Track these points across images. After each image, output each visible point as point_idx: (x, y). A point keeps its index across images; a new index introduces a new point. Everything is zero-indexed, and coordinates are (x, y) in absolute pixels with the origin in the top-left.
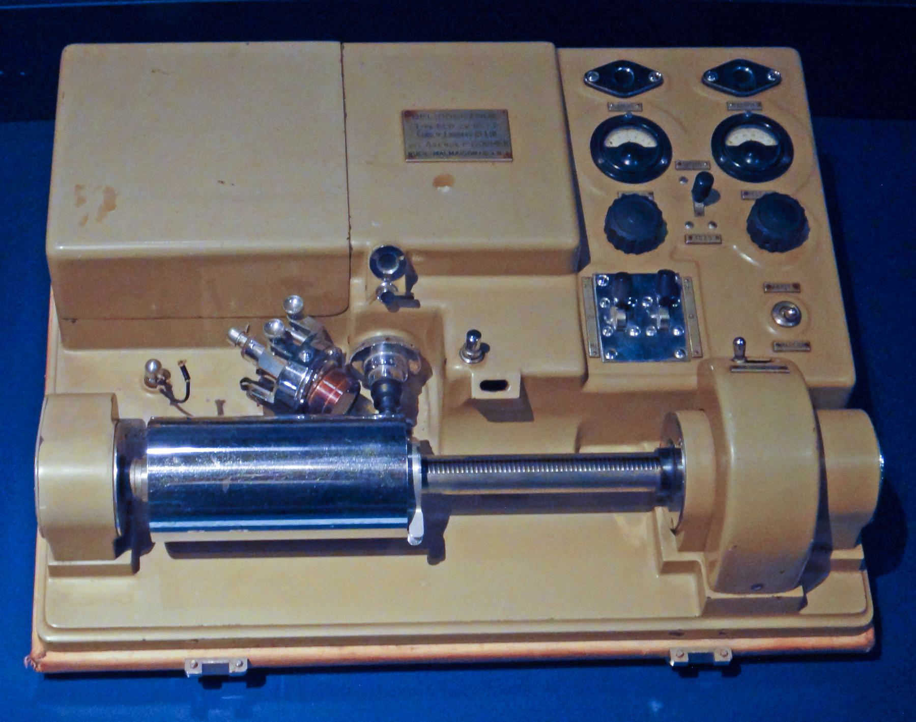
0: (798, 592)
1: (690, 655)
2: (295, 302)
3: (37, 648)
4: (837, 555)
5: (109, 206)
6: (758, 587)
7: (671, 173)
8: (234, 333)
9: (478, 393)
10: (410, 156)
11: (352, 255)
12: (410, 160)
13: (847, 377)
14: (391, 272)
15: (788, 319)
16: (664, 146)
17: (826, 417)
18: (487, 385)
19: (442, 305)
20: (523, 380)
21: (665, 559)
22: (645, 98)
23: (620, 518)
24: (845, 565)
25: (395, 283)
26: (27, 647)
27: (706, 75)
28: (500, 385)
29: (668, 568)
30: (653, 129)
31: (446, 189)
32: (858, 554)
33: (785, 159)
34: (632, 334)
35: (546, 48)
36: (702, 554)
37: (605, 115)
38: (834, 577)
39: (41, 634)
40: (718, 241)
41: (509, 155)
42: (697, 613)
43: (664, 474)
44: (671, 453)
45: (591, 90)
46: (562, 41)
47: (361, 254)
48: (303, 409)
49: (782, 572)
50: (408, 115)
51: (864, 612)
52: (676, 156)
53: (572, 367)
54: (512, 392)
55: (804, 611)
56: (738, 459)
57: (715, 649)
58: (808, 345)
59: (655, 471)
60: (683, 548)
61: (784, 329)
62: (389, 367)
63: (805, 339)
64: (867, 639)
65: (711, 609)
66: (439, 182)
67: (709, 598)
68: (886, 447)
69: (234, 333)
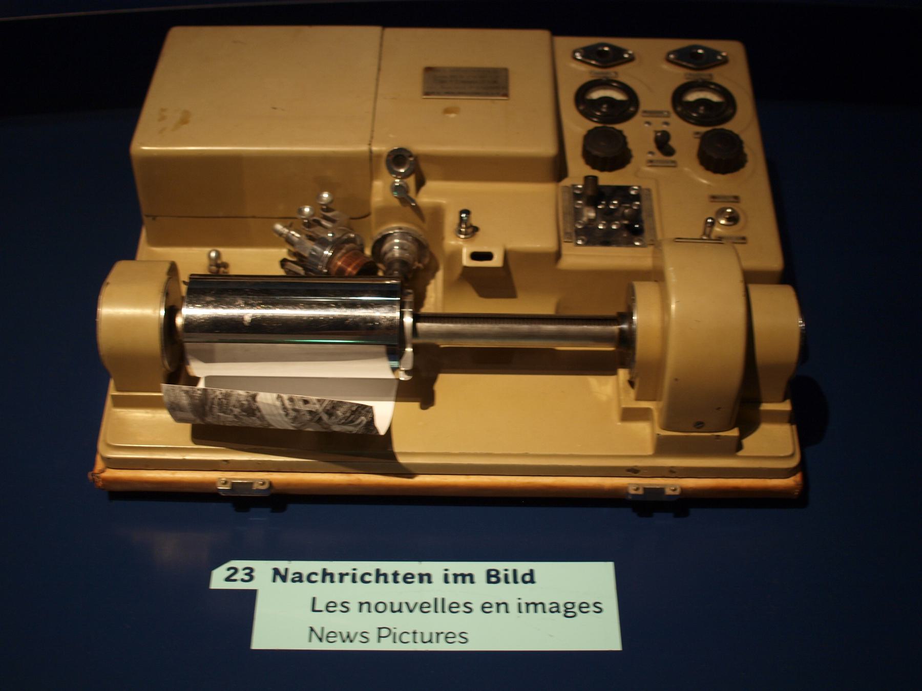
0: (735, 433)
1: (645, 489)
2: (325, 195)
3: (99, 465)
4: (766, 407)
5: (184, 121)
6: (699, 426)
7: (638, 118)
8: (279, 227)
9: (466, 261)
10: (427, 94)
11: (372, 157)
12: (425, 97)
13: (774, 261)
14: (402, 171)
15: (728, 220)
16: (633, 98)
17: (757, 292)
18: (475, 256)
19: (442, 201)
20: (506, 255)
21: (624, 406)
22: (620, 69)
23: (593, 381)
24: (775, 417)
25: (405, 180)
26: (92, 464)
27: (669, 54)
28: (488, 256)
29: (628, 415)
30: (624, 88)
31: (453, 115)
32: (786, 406)
33: (730, 111)
34: (601, 227)
35: (542, 36)
36: (654, 403)
37: (587, 78)
38: (765, 429)
39: (105, 451)
40: (673, 165)
41: (506, 95)
42: (650, 451)
43: (622, 331)
44: (626, 316)
45: (579, 63)
46: (558, 30)
47: (379, 156)
48: (328, 275)
49: (719, 409)
50: (428, 70)
51: (792, 456)
52: (643, 106)
53: (544, 242)
54: (497, 262)
55: (740, 453)
56: (607, 127)
57: (666, 485)
58: (744, 238)
59: (615, 328)
60: (638, 398)
61: (727, 227)
62: (403, 251)
63: (743, 234)
64: (795, 481)
65: (663, 447)
66: (447, 111)
67: (658, 434)
68: (804, 311)
69: (279, 227)
